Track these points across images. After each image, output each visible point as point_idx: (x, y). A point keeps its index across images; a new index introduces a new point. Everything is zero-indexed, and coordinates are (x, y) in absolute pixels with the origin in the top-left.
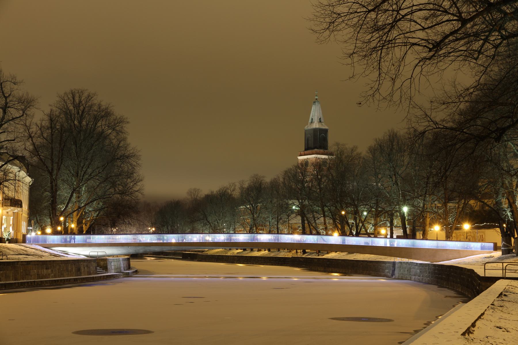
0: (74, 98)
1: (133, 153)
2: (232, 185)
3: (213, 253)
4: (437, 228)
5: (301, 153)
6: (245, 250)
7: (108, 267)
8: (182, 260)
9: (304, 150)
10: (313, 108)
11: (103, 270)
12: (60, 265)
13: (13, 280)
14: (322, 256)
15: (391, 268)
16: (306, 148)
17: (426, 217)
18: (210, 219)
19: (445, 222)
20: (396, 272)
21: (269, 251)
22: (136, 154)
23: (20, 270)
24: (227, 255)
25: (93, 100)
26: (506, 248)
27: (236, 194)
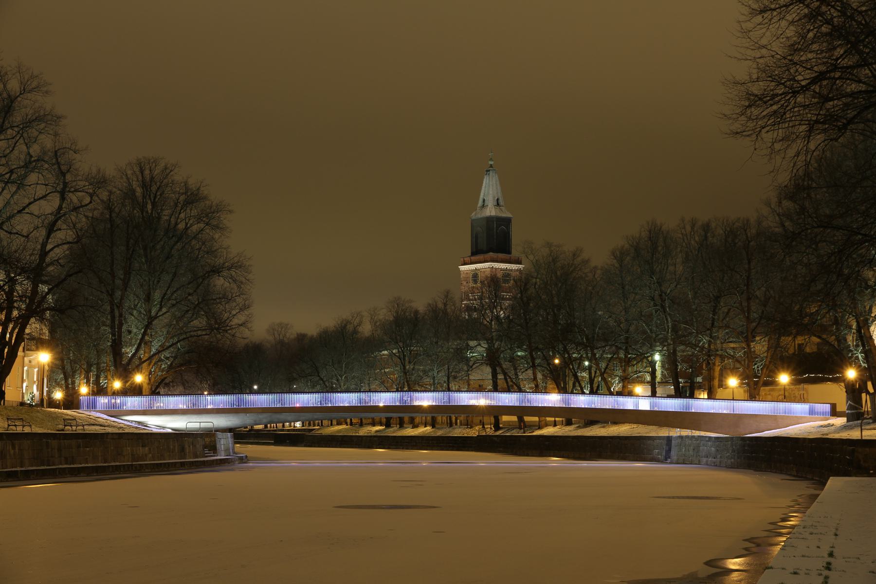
0: (142, 172)
1: (238, 262)
2: (355, 316)
3: (331, 433)
4: (733, 382)
5: (465, 259)
6: (388, 425)
7: (217, 446)
8: (275, 446)
9: (470, 255)
10: (486, 181)
11: (209, 451)
12: (160, 442)
13: (102, 463)
14: (530, 433)
15: (665, 447)
16: (474, 250)
17: (714, 364)
18: (323, 374)
19: (747, 371)
20: (674, 453)
21: (433, 428)
22: (243, 264)
23: (111, 447)
24: (357, 434)
25: (172, 175)
26: (853, 411)
27: (366, 329)
